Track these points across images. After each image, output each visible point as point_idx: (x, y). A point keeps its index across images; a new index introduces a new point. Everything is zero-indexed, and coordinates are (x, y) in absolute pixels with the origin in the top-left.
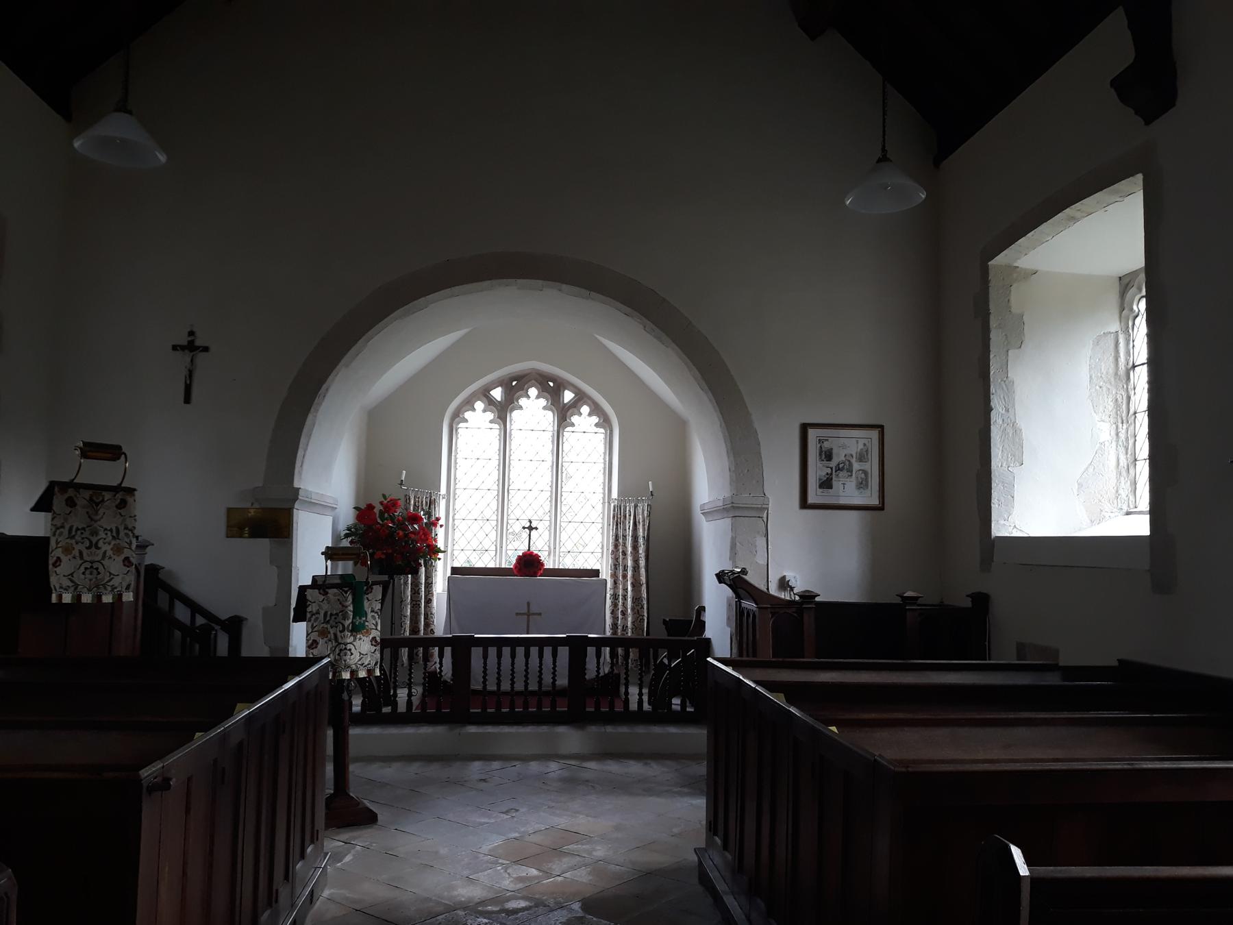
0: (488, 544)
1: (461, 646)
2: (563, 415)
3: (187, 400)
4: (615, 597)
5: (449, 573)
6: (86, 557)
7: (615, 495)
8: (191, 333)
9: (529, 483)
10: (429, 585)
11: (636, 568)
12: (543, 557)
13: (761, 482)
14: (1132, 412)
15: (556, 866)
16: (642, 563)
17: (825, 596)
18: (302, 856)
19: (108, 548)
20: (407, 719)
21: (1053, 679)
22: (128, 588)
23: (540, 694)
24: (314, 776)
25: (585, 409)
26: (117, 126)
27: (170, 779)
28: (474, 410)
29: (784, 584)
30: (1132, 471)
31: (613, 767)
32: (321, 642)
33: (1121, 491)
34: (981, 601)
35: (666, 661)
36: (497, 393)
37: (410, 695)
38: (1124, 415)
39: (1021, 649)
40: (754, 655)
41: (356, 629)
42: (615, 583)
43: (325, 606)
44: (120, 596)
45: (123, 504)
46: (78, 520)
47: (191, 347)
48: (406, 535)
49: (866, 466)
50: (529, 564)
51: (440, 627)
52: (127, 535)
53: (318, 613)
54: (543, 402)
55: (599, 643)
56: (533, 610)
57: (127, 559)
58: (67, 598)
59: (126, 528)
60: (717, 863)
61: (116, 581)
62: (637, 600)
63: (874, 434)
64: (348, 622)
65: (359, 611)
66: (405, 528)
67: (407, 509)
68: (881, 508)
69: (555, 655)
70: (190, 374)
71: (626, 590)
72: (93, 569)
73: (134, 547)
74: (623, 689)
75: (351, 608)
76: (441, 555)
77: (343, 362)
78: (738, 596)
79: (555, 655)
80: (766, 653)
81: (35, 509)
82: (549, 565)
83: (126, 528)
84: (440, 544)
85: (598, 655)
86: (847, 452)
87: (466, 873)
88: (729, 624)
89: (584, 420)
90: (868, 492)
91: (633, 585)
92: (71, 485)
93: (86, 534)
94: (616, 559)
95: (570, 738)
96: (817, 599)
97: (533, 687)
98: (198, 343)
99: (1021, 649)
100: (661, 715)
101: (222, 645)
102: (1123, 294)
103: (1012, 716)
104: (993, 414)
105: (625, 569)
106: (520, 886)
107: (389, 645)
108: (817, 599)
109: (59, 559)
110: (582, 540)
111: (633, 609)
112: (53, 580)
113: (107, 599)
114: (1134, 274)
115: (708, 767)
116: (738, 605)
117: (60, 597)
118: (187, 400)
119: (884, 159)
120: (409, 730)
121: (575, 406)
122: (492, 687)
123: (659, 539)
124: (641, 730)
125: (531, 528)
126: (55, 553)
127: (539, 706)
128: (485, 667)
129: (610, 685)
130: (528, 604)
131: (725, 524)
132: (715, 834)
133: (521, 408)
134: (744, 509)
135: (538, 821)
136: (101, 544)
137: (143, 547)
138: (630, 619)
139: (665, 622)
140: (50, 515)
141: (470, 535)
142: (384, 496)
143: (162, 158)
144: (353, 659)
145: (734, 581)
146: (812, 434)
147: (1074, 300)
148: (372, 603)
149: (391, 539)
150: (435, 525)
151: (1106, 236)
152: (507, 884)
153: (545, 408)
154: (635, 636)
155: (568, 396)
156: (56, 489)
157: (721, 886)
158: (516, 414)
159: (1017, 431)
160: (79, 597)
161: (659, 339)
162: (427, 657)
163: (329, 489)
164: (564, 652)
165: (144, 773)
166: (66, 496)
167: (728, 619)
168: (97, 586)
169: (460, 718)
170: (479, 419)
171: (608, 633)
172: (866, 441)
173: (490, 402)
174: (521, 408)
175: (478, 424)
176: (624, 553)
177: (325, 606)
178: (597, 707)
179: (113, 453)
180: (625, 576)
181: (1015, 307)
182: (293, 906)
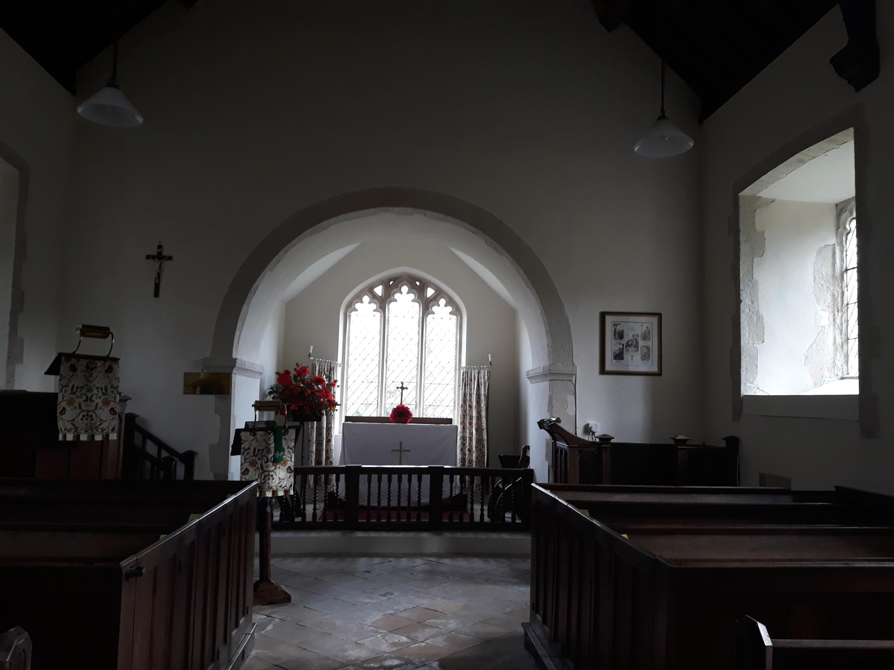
0: (373, 397)
1: (352, 474)
2: (427, 306)
3: (156, 295)
4: (464, 438)
7: (464, 364)
8: (160, 247)
9: (402, 356)
10: (329, 429)
12: (412, 409)
14: (845, 303)
15: (421, 635)
16: (484, 414)
18: (237, 625)
19: (99, 401)
20: (314, 526)
21: (786, 501)
23: (409, 509)
25: (442, 302)
26: (108, 97)
27: (141, 568)
28: (362, 302)
29: (588, 430)
30: (845, 347)
31: (463, 564)
32: (251, 470)
33: (837, 362)
34: (733, 443)
36: (379, 290)
37: (315, 509)
39: (763, 479)
41: (276, 461)
42: (464, 428)
43: (254, 444)
44: (108, 436)
45: (110, 369)
46: (78, 381)
47: (160, 257)
48: (313, 393)
49: (649, 343)
50: (401, 414)
51: (337, 459)
52: (113, 392)
53: (249, 449)
54: (412, 296)
58: (70, 437)
62: (479, 441)
63: (655, 320)
65: (279, 448)
66: (313, 388)
67: (314, 374)
68: (659, 374)
69: (420, 480)
70: (159, 275)
71: (471, 433)
72: (88, 416)
73: (117, 400)
74: (469, 506)
75: (273, 445)
76: (337, 407)
77: (268, 267)
78: (554, 438)
79: (420, 480)
80: (574, 479)
81: (48, 372)
83: (112, 387)
84: (337, 399)
85: (452, 481)
86: (635, 333)
87: (355, 639)
88: (547, 459)
89: (442, 310)
91: (477, 430)
92: (73, 355)
93: (84, 391)
94: (464, 411)
95: (432, 542)
96: (612, 441)
97: (404, 503)
98: (165, 253)
99: (763, 479)
100: (497, 525)
101: (180, 471)
104: (742, 305)
105: (471, 418)
106: (395, 649)
107: (300, 473)
108: (612, 441)
109: (64, 409)
110: (440, 397)
111: (476, 447)
112: (60, 424)
113: (98, 438)
116: (554, 444)
117: (65, 436)
118: (156, 295)
119: (662, 117)
120: (314, 535)
121: (435, 299)
122: (374, 503)
123: (496, 396)
124: (482, 536)
125: (402, 388)
126: (62, 404)
129: (460, 503)
130: (401, 443)
131: (545, 385)
132: (537, 612)
133: (396, 301)
134: (558, 374)
135: (407, 602)
137: (124, 400)
138: (474, 455)
140: (58, 377)
141: (359, 395)
142: (297, 364)
143: (140, 120)
144: (274, 483)
145: (552, 428)
146: (609, 320)
147: (802, 221)
148: (289, 441)
149: (302, 396)
150: (333, 385)
151: (827, 174)
153: (413, 301)
155: (430, 292)
157: (541, 651)
158: (392, 305)
159: (760, 318)
160: (78, 436)
162: (327, 481)
164: (426, 478)
165: (124, 563)
169: (351, 526)
170: (366, 309)
173: (374, 297)
174: (396, 301)
176: (470, 407)
177: (254, 444)
178: (451, 519)
179: (103, 332)
180: (471, 424)
181: (759, 227)
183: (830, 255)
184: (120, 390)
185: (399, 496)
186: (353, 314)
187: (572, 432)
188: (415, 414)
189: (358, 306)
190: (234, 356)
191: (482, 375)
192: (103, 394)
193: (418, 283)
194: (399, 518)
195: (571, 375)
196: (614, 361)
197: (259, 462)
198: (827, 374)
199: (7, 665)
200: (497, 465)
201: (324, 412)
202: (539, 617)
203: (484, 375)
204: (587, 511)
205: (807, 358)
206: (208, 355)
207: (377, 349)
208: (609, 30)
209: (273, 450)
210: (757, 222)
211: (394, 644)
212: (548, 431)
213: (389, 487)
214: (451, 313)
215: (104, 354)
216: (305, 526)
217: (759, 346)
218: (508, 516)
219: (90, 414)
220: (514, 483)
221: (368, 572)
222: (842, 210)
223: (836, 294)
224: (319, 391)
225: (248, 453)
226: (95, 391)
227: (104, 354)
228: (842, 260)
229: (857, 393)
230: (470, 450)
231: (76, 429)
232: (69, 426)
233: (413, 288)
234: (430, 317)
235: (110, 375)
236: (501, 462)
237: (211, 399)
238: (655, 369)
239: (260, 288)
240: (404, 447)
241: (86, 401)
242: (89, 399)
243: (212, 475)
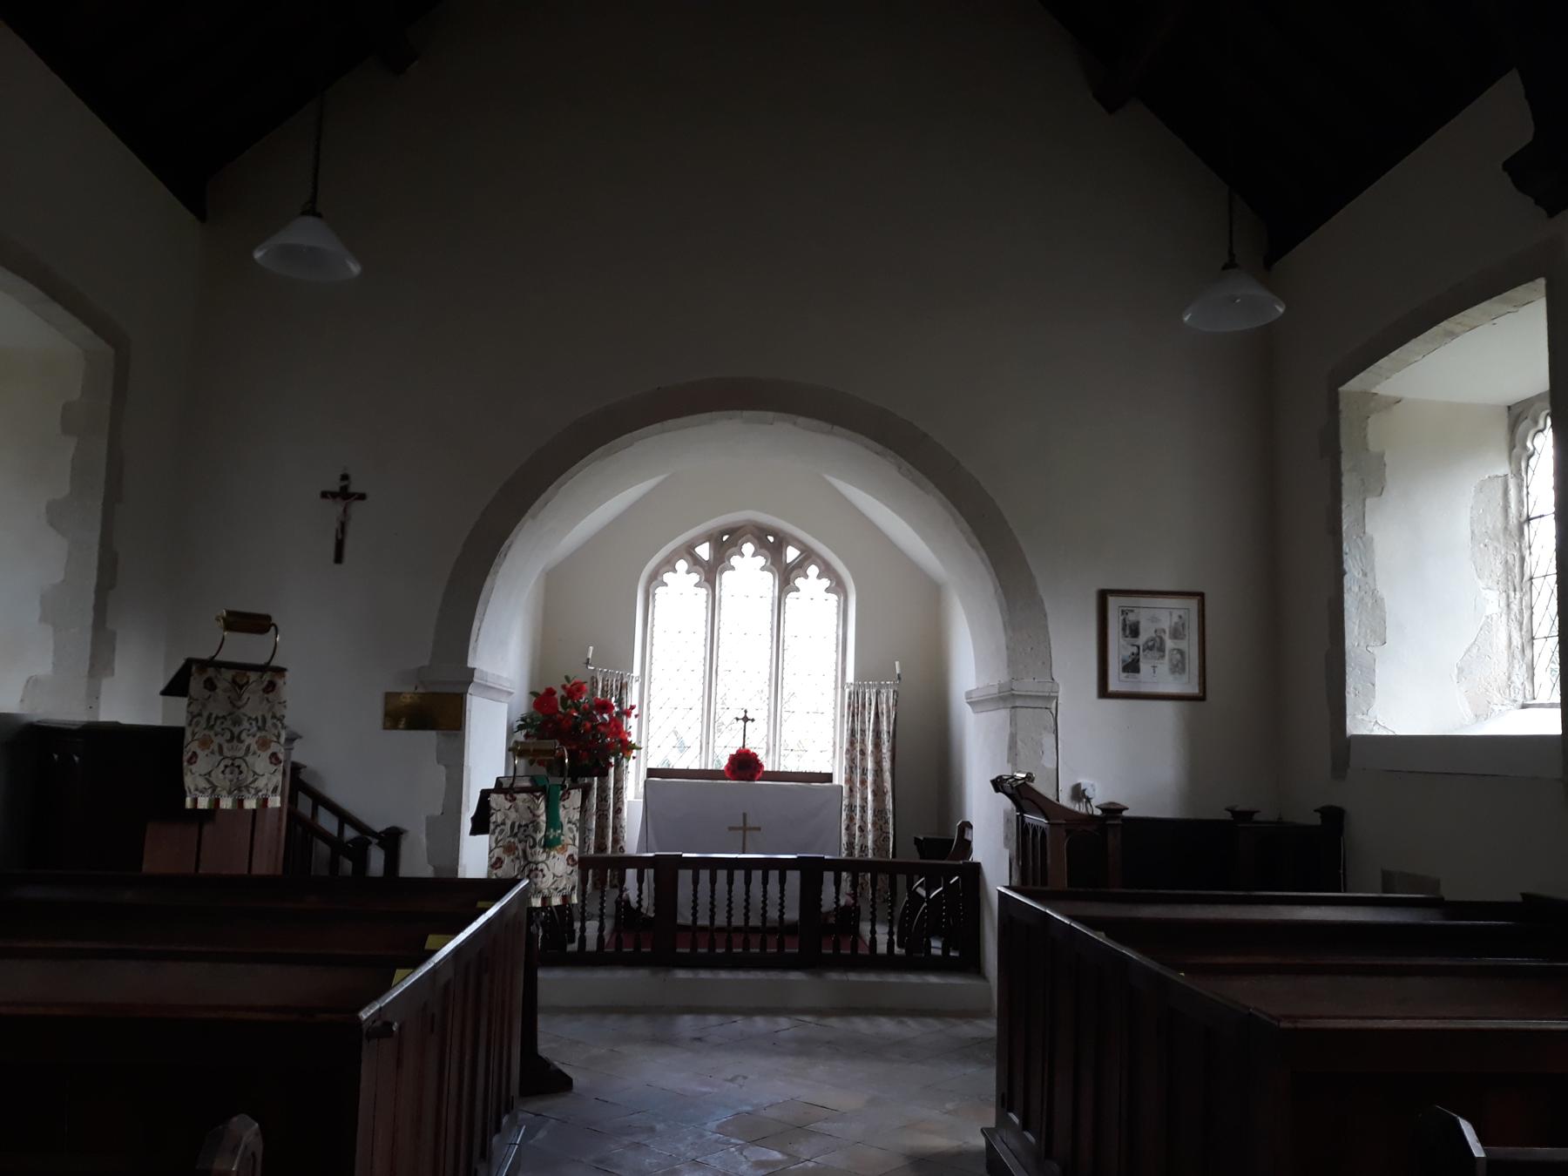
0: (693, 737)
1: (665, 869)
2: (786, 577)
3: (339, 558)
4: (851, 808)
6: (227, 753)
7: (850, 678)
8: (345, 477)
9: (745, 661)
10: (619, 790)
12: (761, 757)
13: (1048, 663)
14: (1526, 577)
15: (804, 1149)
16: (887, 765)
17: (1135, 809)
18: (498, 1129)
21: (1431, 918)
22: (275, 790)
23: (764, 930)
24: (627, 1011)
25: (813, 570)
26: (306, 233)
27: (391, 1024)
28: (675, 571)
29: (1078, 793)
30: (1528, 652)
31: (861, 1025)
32: (507, 860)
33: (1514, 678)
34: (1334, 817)
35: (923, 892)
36: (704, 551)
37: (601, 929)
38: (1517, 580)
39: (1388, 881)
40: (1045, 883)
41: (549, 844)
42: (851, 790)
43: (513, 815)
44: (265, 801)
45: (271, 687)
46: (218, 707)
47: (344, 494)
48: (593, 727)
49: (1183, 645)
50: (744, 764)
51: (632, 842)
52: (275, 725)
53: (503, 823)
54: (761, 561)
55: (837, 866)
56: (750, 823)
57: (274, 755)
58: (203, 803)
59: (274, 717)
61: (261, 783)
62: (879, 812)
63: (1193, 604)
64: (540, 836)
65: (553, 822)
66: (593, 719)
67: (594, 694)
68: (1201, 698)
70: (343, 527)
71: (864, 799)
72: (235, 767)
73: (282, 740)
74: (577, 925)
77: (530, 512)
78: (1020, 808)
80: (1059, 878)
81: (167, 692)
82: (768, 767)
83: (274, 717)
84: (633, 739)
87: (691, 1154)
88: (1006, 845)
89: (812, 584)
90: (1185, 678)
91: (875, 793)
92: (211, 663)
93: (228, 723)
94: (852, 760)
96: (1125, 813)
97: (755, 921)
98: (353, 489)
99: (1388, 881)
100: (917, 961)
101: (376, 861)
102: (1513, 427)
103: (1405, 961)
104: (1347, 579)
105: (864, 772)
107: (583, 864)
108: (1125, 813)
111: (874, 824)
112: (189, 781)
113: (251, 804)
114: (1539, 397)
115: (999, 1025)
116: (1021, 821)
117: (195, 801)
118: (339, 558)
119: (1230, 265)
120: (601, 975)
121: (800, 567)
122: (703, 921)
123: (911, 740)
124: (892, 978)
125: (746, 719)
126: (191, 746)
127: (763, 946)
129: (847, 918)
131: (1001, 716)
133: (733, 568)
134: (1022, 698)
136: (244, 736)
137: (291, 739)
138: (870, 837)
139: (917, 841)
140: (185, 701)
141: (673, 726)
142: (567, 678)
143: (355, 269)
144: (546, 883)
145: (1019, 792)
146: (1114, 603)
147: (1450, 436)
149: (575, 734)
150: (628, 714)
153: (763, 569)
154: (878, 859)
155: (792, 554)
158: (727, 575)
159: (1378, 602)
160: (217, 801)
161: (918, 484)
164: (794, 877)
165: (365, 1015)
166: (205, 676)
167: (1006, 838)
168: (239, 789)
170: (681, 584)
172: (1181, 613)
173: (696, 562)
174: (733, 568)
175: (677, 597)
176: (863, 753)
177: (513, 815)
178: (837, 948)
179: (258, 624)
180: (863, 782)
181: (1373, 446)
183: (1500, 494)
184: (286, 721)
185: (747, 908)
186: (660, 591)
187: (1051, 796)
189: (668, 577)
192: (259, 729)
193: (771, 539)
195: (1049, 698)
197: (520, 847)
198: (1497, 698)
200: (913, 856)
201: (612, 760)
203: (888, 697)
205: (1461, 670)
206: (426, 663)
207: (700, 652)
208: (1111, 108)
209: (543, 826)
210: (1370, 437)
213: (730, 891)
214: (827, 590)
215: (262, 661)
216: (584, 960)
217: (1377, 651)
218: (936, 946)
220: (947, 886)
221: (699, 1039)
222: (1519, 416)
223: (1511, 561)
224: (604, 724)
226: (246, 724)
228: (1520, 502)
229: (1559, 732)
232: (203, 784)
233: (762, 546)
235: (271, 696)
237: (428, 739)
238: (1193, 689)
242: (235, 738)
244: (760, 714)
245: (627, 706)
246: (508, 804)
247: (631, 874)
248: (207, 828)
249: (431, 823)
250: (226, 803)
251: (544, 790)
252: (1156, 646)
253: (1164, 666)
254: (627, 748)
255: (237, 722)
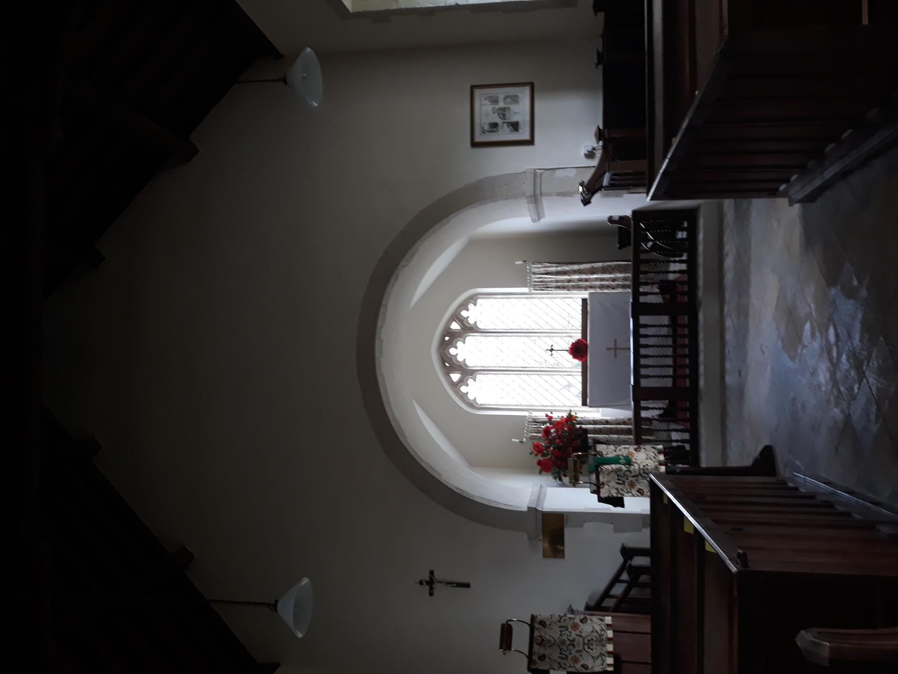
1: (641, 395)
2: (469, 329)
3: (467, 586)
4: (602, 287)
5: (585, 408)
6: (581, 648)
7: (526, 290)
10: (595, 422)
11: (580, 272)
16: (576, 267)
18: (796, 489)
23: (675, 336)
25: (464, 313)
26: (286, 610)
27: (739, 554)
29: (590, 155)
32: (638, 486)
35: (650, 244)
36: (455, 377)
37: (677, 430)
40: (644, 173)
41: (629, 462)
42: (591, 287)
43: (613, 484)
44: (608, 625)
45: (542, 623)
47: (431, 583)
49: (501, 97)
50: (578, 350)
51: (626, 414)
52: (565, 620)
54: (459, 344)
55: (636, 294)
56: (612, 346)
57: (582, 621)
58: (610, 660)
59: (560, 621)
60: (800, 190)
61: (598, 628)
62: (604, 270)
63: (477, 92)
65: (615, 460)
66: (554, 438)
67: (540, 438)
68: (532, 86)
69: (645, 326)
70: (448, 583)
71: (596, 279)
72: (589, 643)
73: (572, 616)
74: (674, 444)
76: (573, 414)
77: (437, 477)
78: (599, 189)
79: (645, 326)
80: (641, 165)
82: (579, 336)
83: (560, 621)
84: (565, 415)
89: (472, 314)
90: (520, 95)
91: (593, 273)
94: (574, 287)
96: (601, 127)
97: (670, 341)
98: (427, 578)
101: (644, 578)
106: (818, 334)
107: (639, 442)
108: (601, 127)
110: (560, 313)
111: (611, 273)
112: (598, 669)
113: (610, 634)
116: (607, 188)
117: (609, 665)
118: (467, 586)
119: (284, 81)
120: (703, 431)
121: (462, 321)
122: (670, 371)
124: (701, 260)
128: (655, 377)
130: (608, 349)
131: (545, 201)
132: (777, 190)
136: (571, 638)
137: (572, 611)
139: (620, 248)
141: (557, 392)
143: (305, 581)
144: (651, 464)
145: (591, 190)
146: (478, 138)
148: (608, 451)
149: (563, 449)
150: (550, 418)
152: (816, 345)
154: (631, 271)
155: (455, 326)
156: (533, 667)
157: (818, 182)
158: (468, 363)
160: (609, 653)
162: (649, 420)
163: (525, 491)
164: (643, 320)
165: (734, 569)
166: (538, 660)
167: (617, 196)
170: (474, 390)
171: (630, 290)
173: (462, 381)
175: (479, 391)
176: (569, 281)
178: (684, 293)
179: (507, 632)
180: (586, 280)
182: (833, 493)
187: (592, 171)
188: (579, 336)
189: (471, 397)
190: (525, 509)
191: (536, 270)
192: (567, 629)
194: (684, 356)
195: (535, 174)
196: (520, 131)
197: (631, 479)
199: (832, 645)
201: (578, 426)
202: (782, 187)
203: (537, 268)
204: (674, 140)
206: (525, 536)
207: (513, 377)
211: (813, 334)
212: (593, 194)
214: (475, 305)
215: (528, 629)
216: (694, 441)
219: (586, 641)
220: (647, 229)
224: (556, 432)
225: (622, 490)
226: (565, 637)
227: (527, 629)
230: (614, 280)
231: (601, 654)
232: (599, 661)
233: (451, 344)
234: (480, 326)
235: (548, 623)
236: (625, 246)
237: (569, 534)
238: (527, 90)
239: (457, 485)
240: (612, 346)
241: (574, 646)
242: (572, 643)
243: (644, 530)
244: (548, 342)
245: (546, 419)
246: (606, 487)
247: (644, 414)
248: (624, 658)
249: (616, 530)
250: (610, 647)
251: (597, 467)
252: (503, 113)
253: (514, 108)
254: (570, 418)
255: (563, 642)
